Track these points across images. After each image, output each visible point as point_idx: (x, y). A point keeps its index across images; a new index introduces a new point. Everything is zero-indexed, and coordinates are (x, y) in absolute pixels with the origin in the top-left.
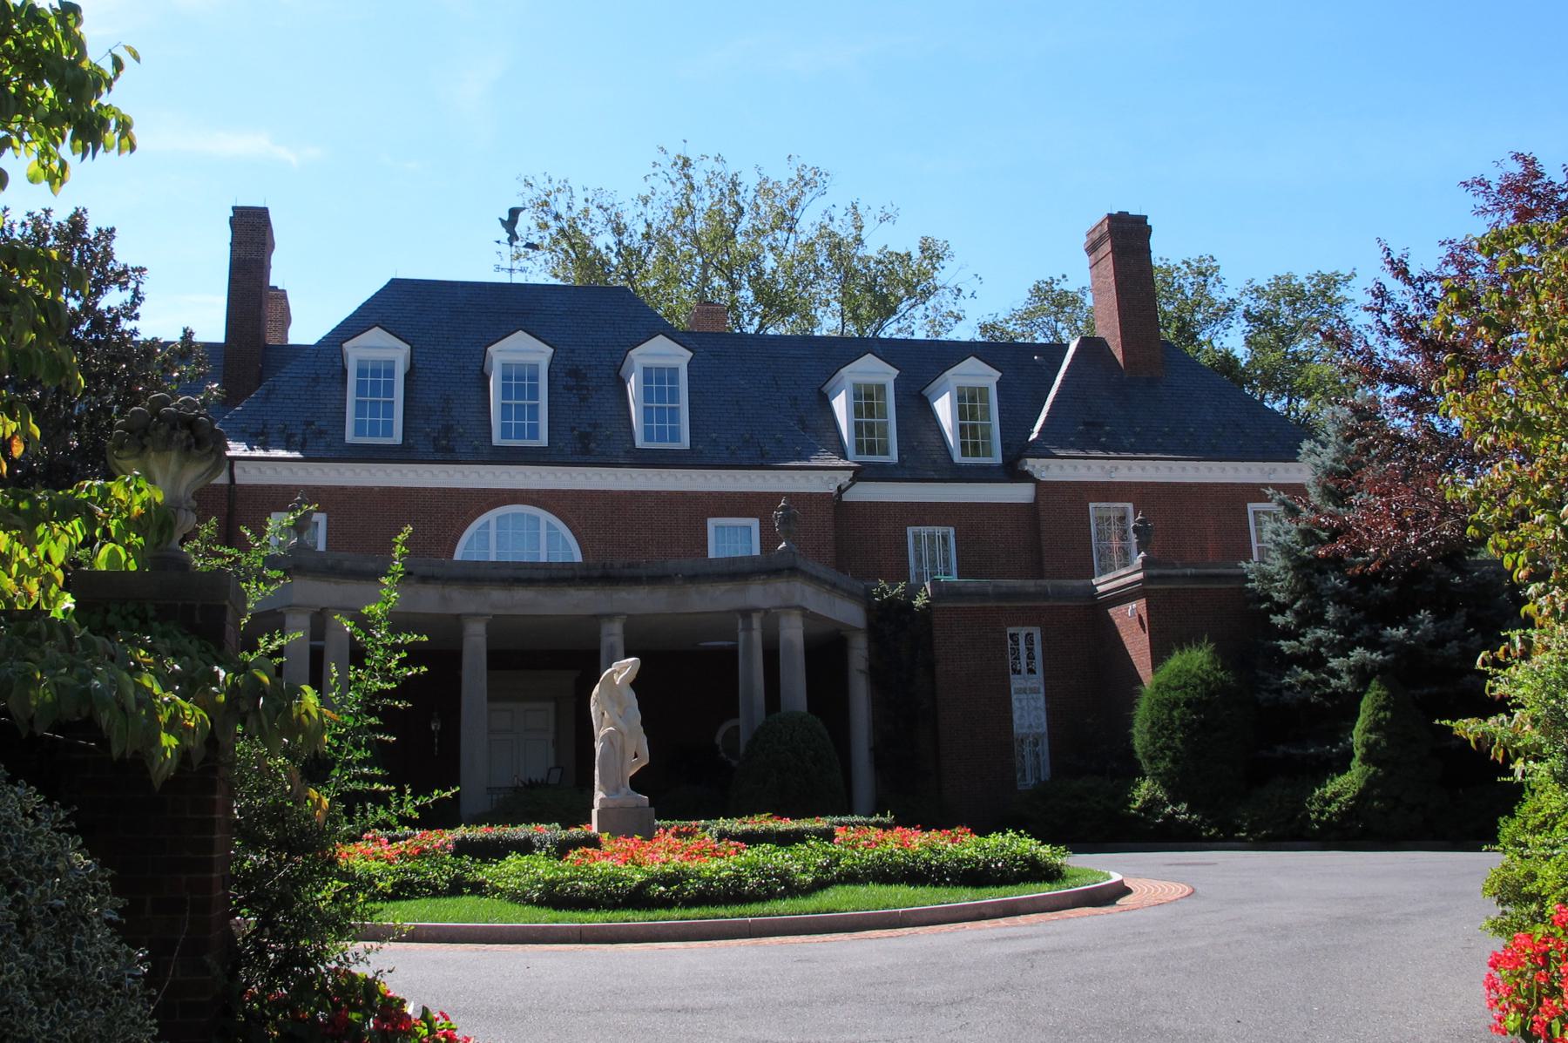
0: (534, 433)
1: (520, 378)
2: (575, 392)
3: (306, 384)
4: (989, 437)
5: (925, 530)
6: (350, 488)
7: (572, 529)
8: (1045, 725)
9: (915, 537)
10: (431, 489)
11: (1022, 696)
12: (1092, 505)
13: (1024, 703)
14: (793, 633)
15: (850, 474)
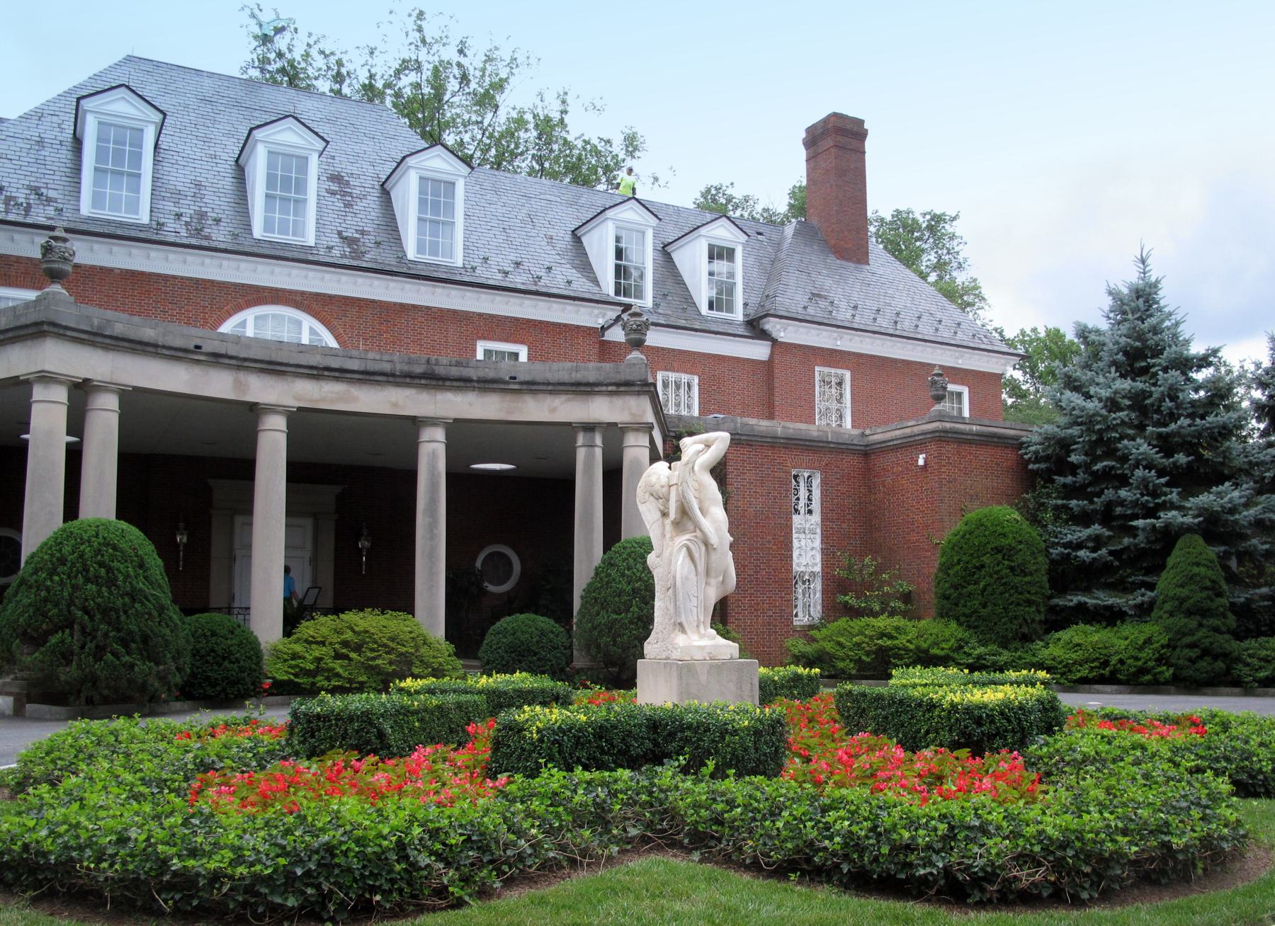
2: (338, 197)
3: (29, 146)
6: (85, 266)
8: (820, 565)
10: (182, 278)
12: (817, 369)
13: (803, 542)
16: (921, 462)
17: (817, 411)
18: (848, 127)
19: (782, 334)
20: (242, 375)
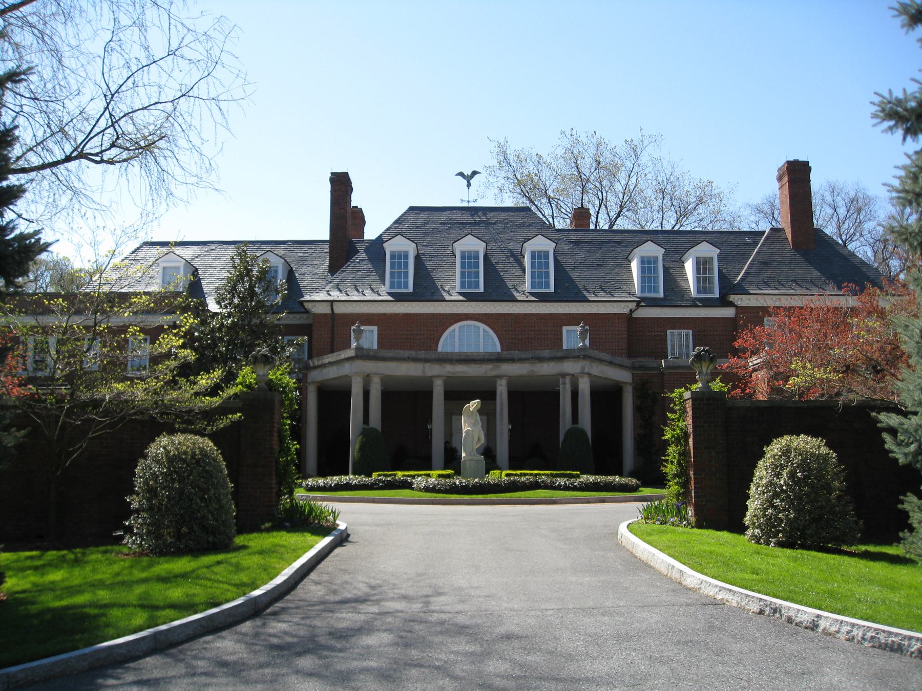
0: (477, 286)
1: (470, 258)
4: (713, 283)
5: (676, 332)
7: (496, 332)
9: (671, 335)
14: (584, 386)
15: (635, 304)
19: (739, 303)
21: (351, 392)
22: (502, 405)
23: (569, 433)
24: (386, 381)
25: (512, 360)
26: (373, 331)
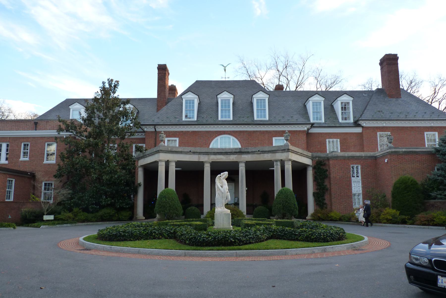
8: (361, 191)
11: (355, 183)
12: (378, 133)
14: (289, 167)
16: (386, 161)
17: (379, 145)
18: (391, 57)
19: (364, 125)
20: (200, 155)
21: (157, 172)
22: (242, 177)
23: (281, 192)
24: (178, 164)
25: (248, 153)
26: (176, 140)
